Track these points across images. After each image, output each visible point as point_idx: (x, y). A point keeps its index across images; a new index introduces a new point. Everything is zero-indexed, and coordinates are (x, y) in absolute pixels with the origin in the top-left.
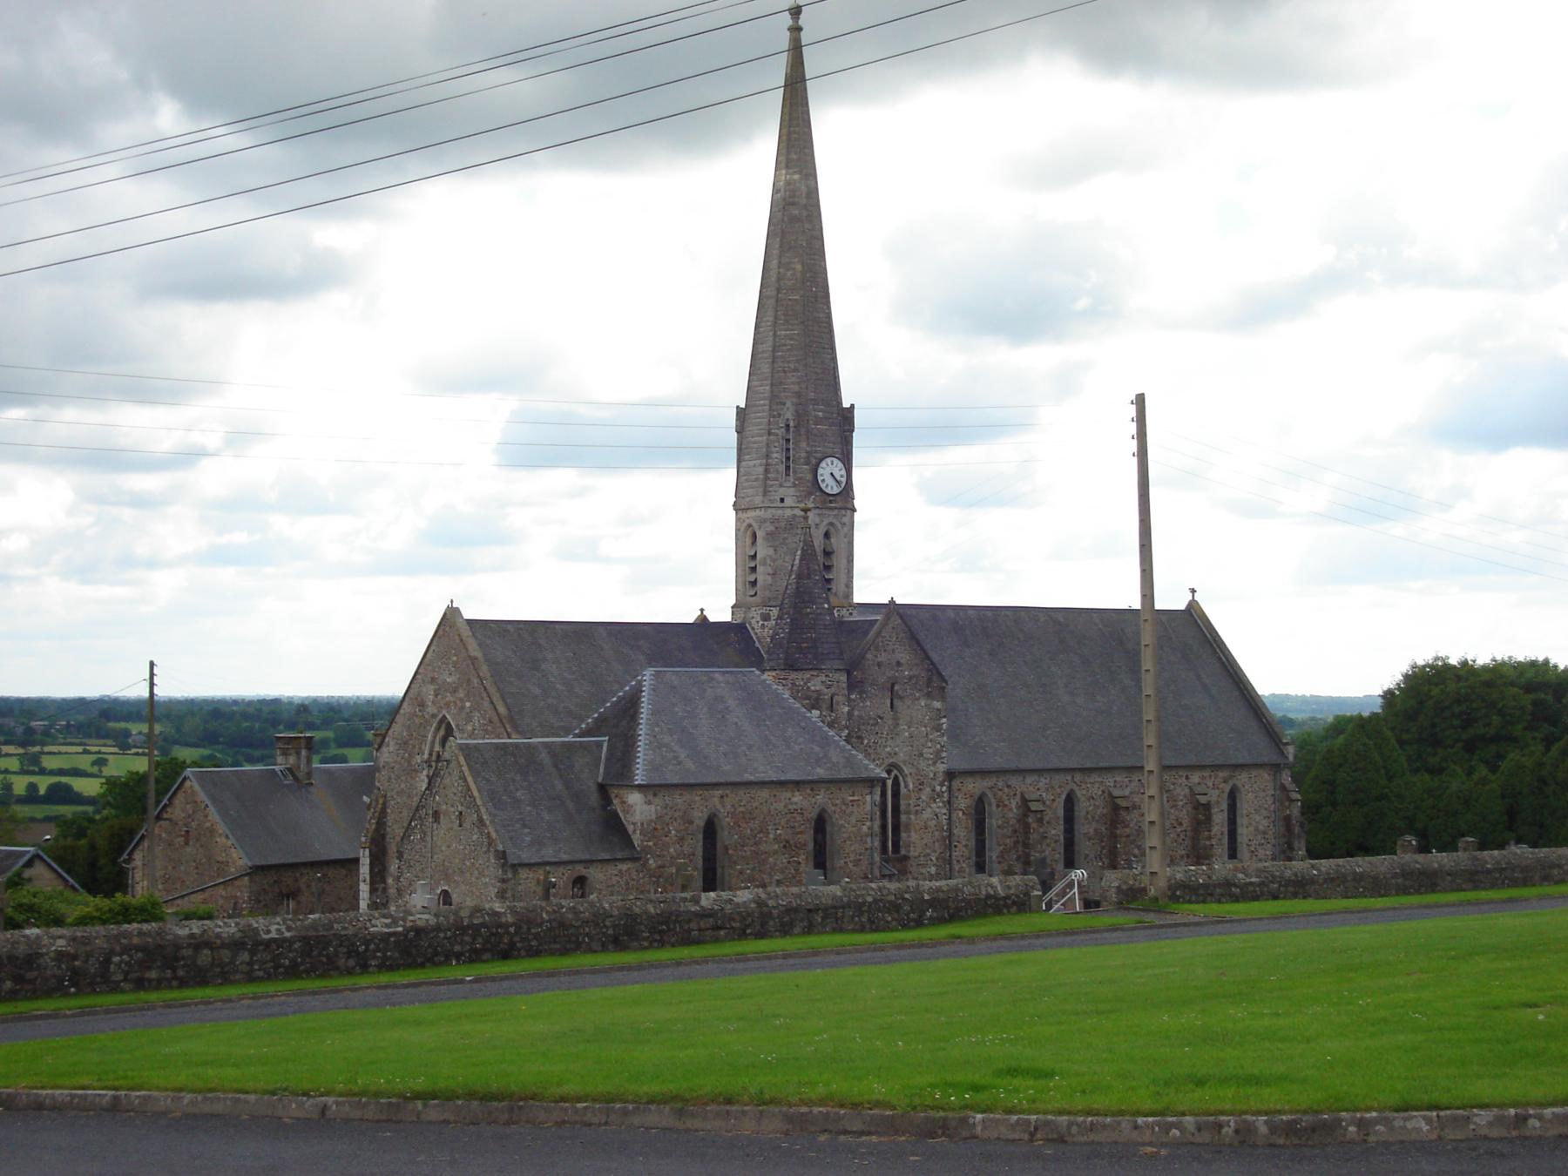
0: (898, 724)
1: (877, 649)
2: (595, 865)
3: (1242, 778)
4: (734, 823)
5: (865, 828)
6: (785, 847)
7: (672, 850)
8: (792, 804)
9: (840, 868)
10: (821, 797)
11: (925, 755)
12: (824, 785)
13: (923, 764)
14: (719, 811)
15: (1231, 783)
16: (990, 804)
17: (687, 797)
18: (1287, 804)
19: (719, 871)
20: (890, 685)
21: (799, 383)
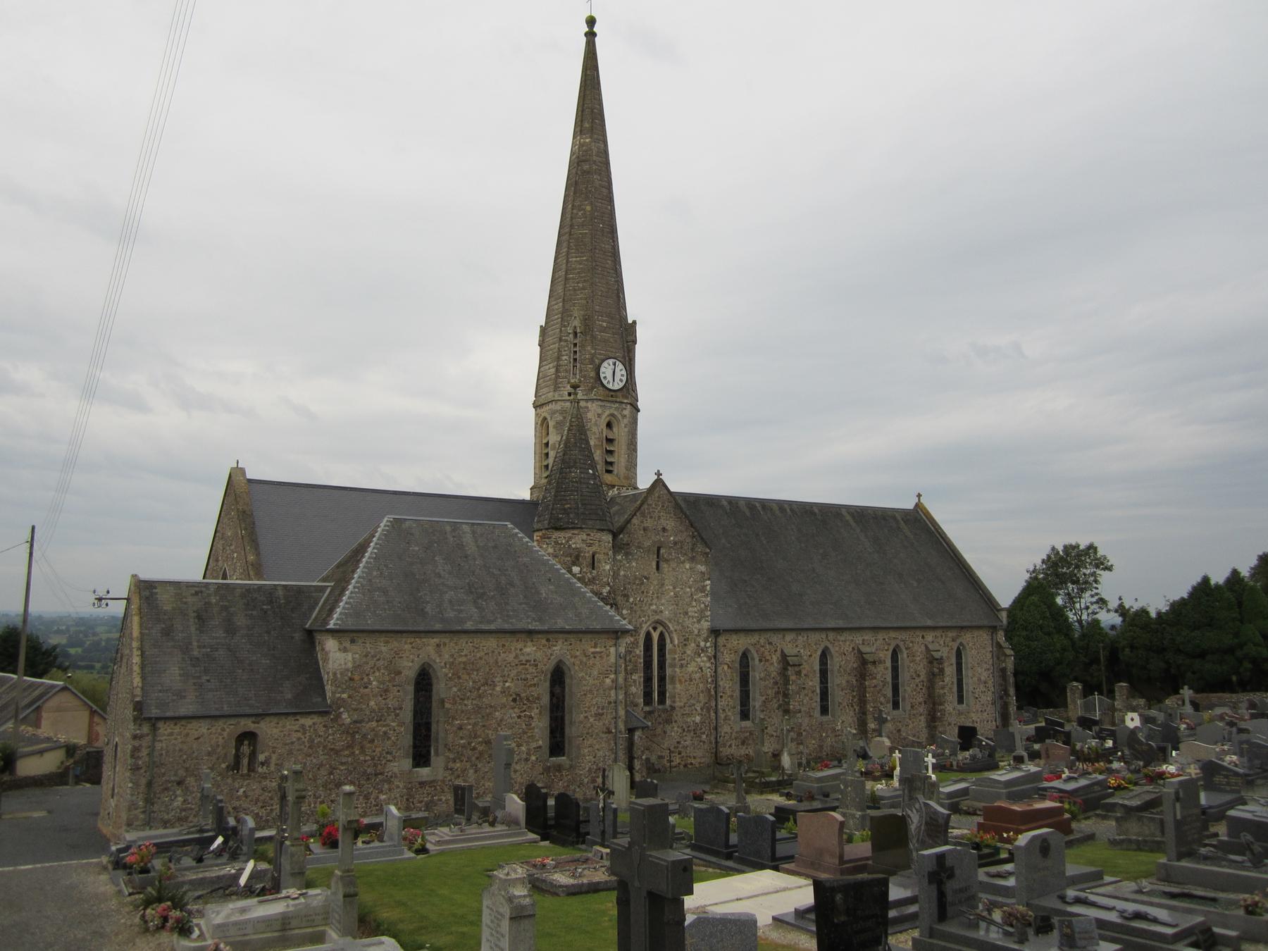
0: (663, 584)
1: (643, 515)
2: (268, 719)
3: (967, 638)
4: (453, 675)
5: (608, 681)
6: (514, 700)
7: (372, 703)
8: (523, 654)
9: (581, 722)
10: (559, 649)
11: (690, 614)
12: (561, 636)
13: (688, 622)
14: (435, 661)
15: (958, 641)
16: (753, 659)
17: (395, 644)
18: (1003, 658)
19: (434, 727)
20: (656, 549)
21: (586, 299)
